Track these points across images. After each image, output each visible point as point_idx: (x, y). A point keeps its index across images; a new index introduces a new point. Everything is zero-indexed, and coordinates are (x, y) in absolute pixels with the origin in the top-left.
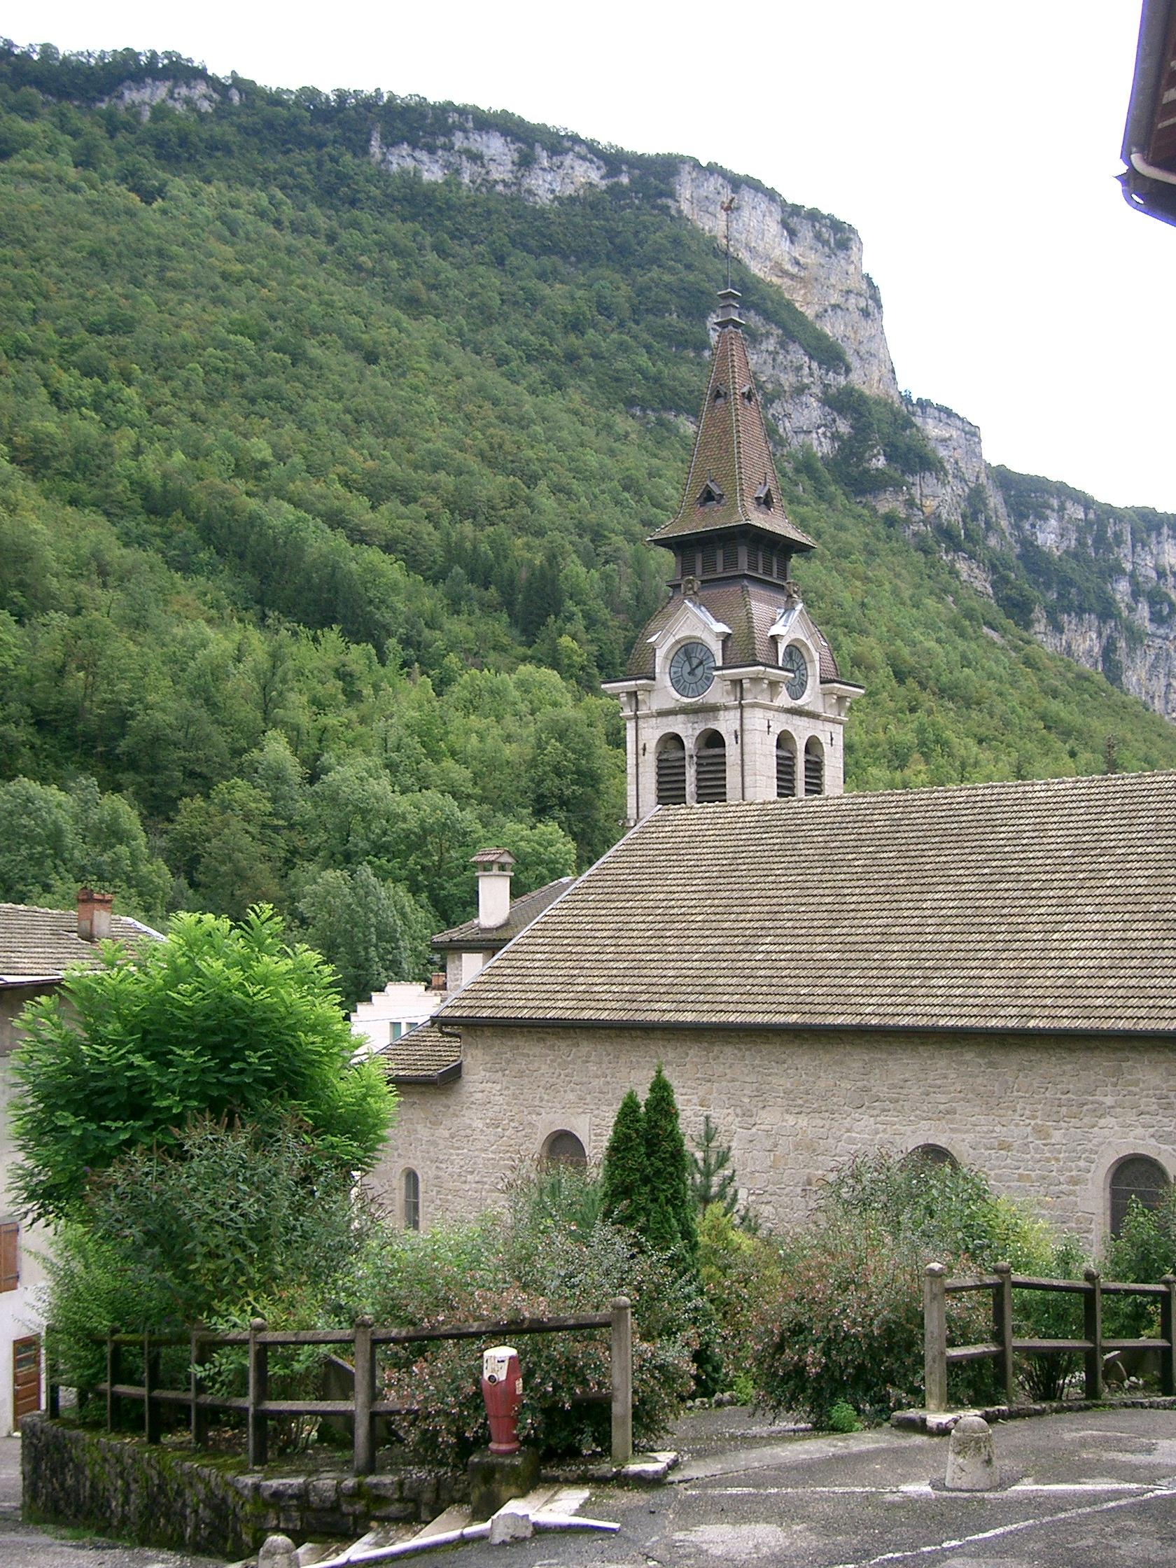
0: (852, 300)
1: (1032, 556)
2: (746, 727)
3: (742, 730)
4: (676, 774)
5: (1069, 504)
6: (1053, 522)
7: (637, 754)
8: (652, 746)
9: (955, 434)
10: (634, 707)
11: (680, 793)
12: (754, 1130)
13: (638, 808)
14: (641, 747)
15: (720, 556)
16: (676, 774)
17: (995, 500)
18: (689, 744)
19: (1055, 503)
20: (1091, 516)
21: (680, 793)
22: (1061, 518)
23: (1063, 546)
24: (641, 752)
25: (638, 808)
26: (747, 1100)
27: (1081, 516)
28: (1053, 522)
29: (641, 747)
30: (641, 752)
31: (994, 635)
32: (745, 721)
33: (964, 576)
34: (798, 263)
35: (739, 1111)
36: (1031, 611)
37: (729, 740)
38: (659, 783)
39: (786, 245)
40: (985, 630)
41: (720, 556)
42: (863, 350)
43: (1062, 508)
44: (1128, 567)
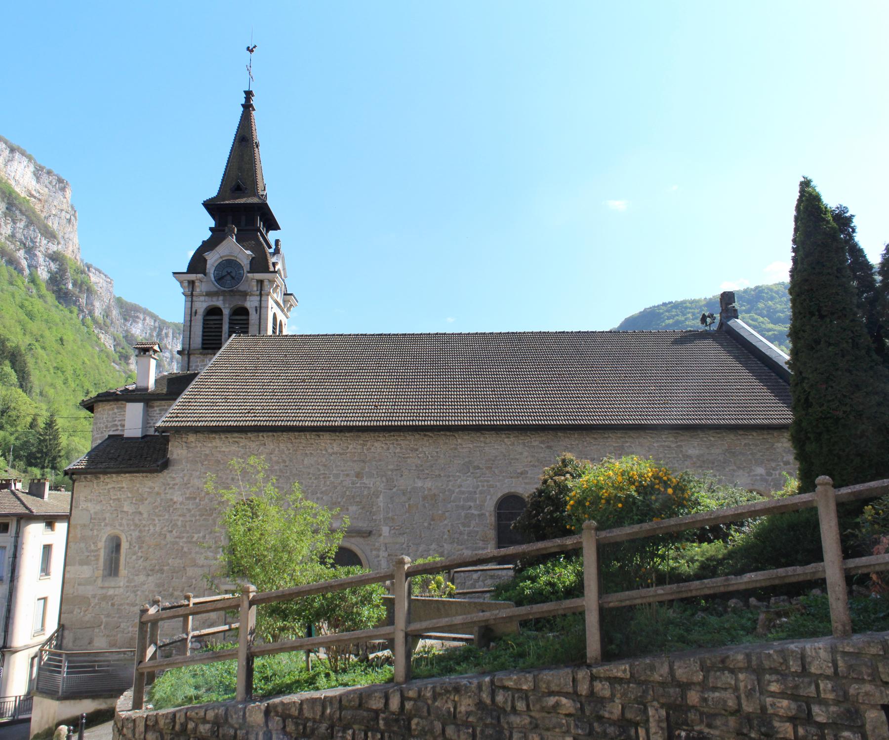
0: (64, 213)
1: (128, 337)
2: (262, 305)
3: (260, 307)
4: (208, 328)
5: (148, 318)
6: (140, 325)
7: (191, 315)
8: (201, 311)
9: (101, 281)
10: (191, 289)
11: (219, 334)
12: (394, 490)
13: (190, 338)
14: (194, 311)
15: (243, 218)
16: (208, 328)
17: (115, 313)
18: (226, 312)
19: (142, 316)
20: (157, 325)
21: (219, 334)
22: (143, 324)
23: (144, 335)
24: (193, 314)
25: (190, 338)
26: (390, 473)
27: (152, 324)
28: (140, 325)
29: (194, 311)
30: (193, 314)
31: (115, 365)
32: (262, 302)
33: (102, 341)
34: (39, 192)
35: (384, 479)
36: (130, 359)
37: (252, 312)
38: (203, 332)
39: (34, 182)
40: (113, 364)
41: (243, 218)
42: (66, 236)
43: (144, 319)
44: (170, 347)
